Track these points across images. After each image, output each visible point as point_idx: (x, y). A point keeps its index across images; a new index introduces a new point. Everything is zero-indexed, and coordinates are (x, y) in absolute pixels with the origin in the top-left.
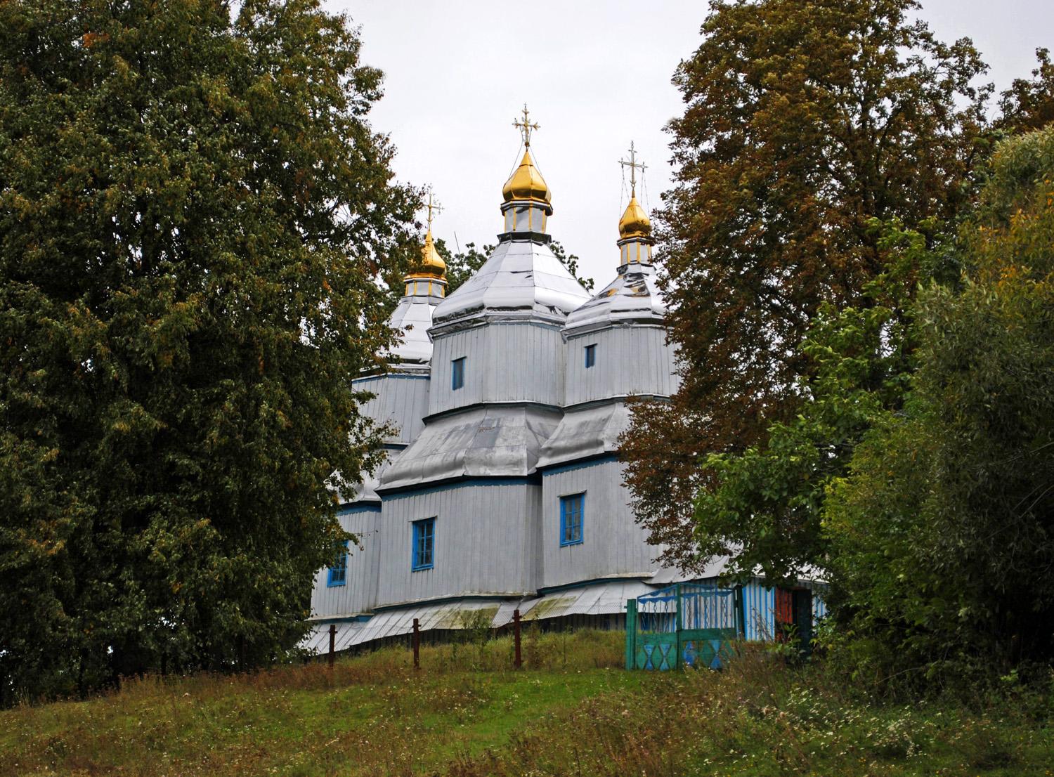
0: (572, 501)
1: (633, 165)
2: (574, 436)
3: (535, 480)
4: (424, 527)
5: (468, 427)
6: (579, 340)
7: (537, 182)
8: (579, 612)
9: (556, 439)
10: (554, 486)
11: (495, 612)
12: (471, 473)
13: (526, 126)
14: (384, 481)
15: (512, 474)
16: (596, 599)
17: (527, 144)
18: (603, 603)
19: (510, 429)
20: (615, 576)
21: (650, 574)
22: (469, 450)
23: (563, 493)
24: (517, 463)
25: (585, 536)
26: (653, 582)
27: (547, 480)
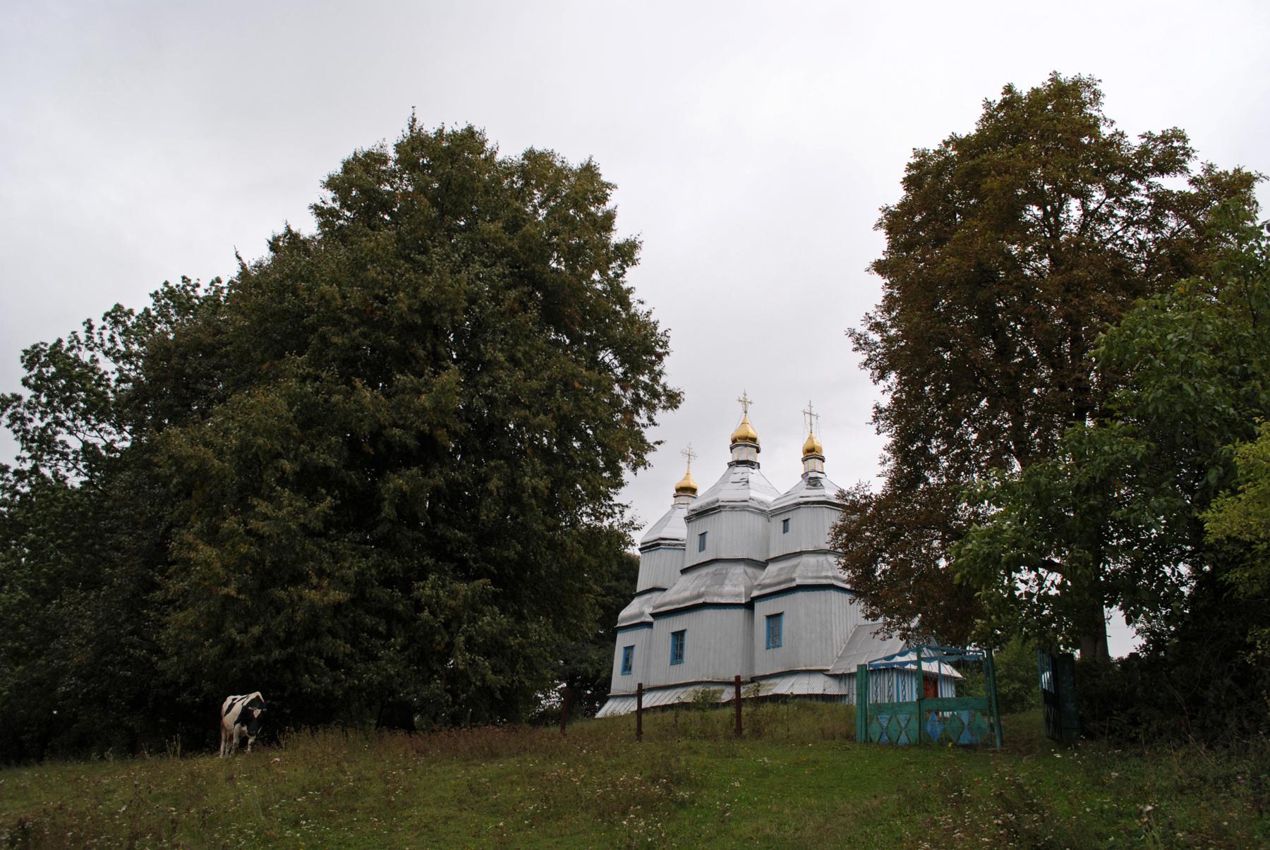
0: (774, 618)
1: (811, 414)
2: (775, 577)
3: (749, 606)
4: (679, 636)
5: (707, 574)
6: (778, 517)
7: (752, 433)
8: (779, 692)
9: (764, 579)
10: (763, 609)
11: (722, 692)
12: (708, 601)
13: (745, 402)
14: (655, 608)
15: (734, 602)
16: (790, 684)
17: (746, 412)
18: (795, 686)
19: (734, 574)
20: (804, 668)
21: (828, 668)
22: (708, 586)
23: (768, 614)
24: (738, 595)
25: (783, 641)
26: (830, 673)
27: (758, 606)
